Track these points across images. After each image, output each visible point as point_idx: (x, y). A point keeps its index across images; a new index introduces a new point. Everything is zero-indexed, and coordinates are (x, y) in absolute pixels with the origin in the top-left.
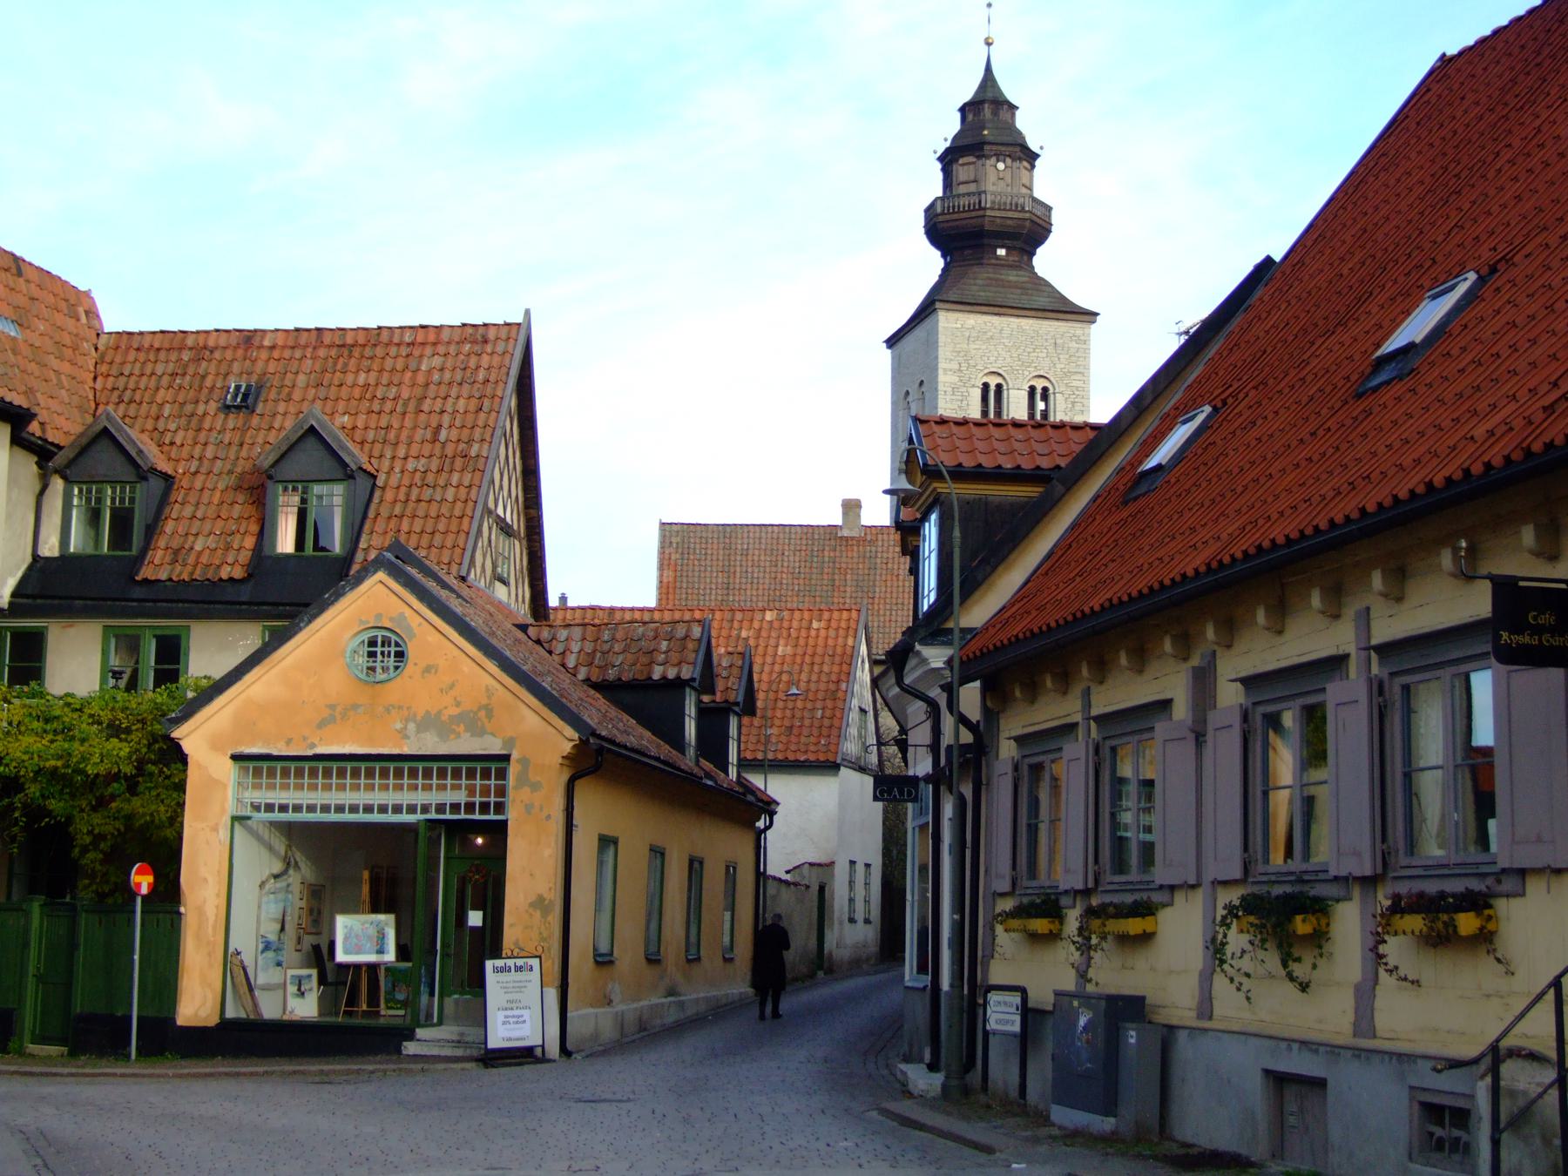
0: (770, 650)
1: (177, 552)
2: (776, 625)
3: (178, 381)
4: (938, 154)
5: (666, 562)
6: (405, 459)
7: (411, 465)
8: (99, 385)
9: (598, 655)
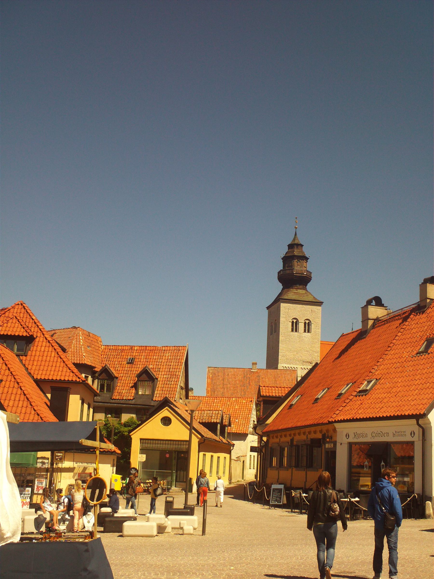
0: (234, 407)
1: (119, 393)
2: (235, 401)
3: (118, 357)
4: (282, 258)
5: (209, 377)
6: (164, 375)
7: (165, 376)
8: (102, 357)
9: (201, 417)
